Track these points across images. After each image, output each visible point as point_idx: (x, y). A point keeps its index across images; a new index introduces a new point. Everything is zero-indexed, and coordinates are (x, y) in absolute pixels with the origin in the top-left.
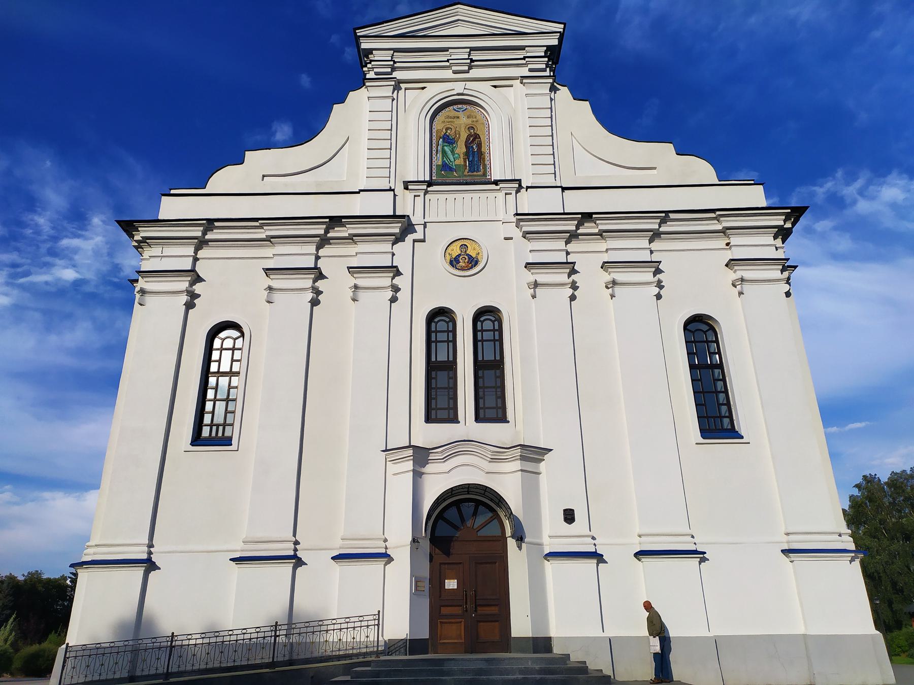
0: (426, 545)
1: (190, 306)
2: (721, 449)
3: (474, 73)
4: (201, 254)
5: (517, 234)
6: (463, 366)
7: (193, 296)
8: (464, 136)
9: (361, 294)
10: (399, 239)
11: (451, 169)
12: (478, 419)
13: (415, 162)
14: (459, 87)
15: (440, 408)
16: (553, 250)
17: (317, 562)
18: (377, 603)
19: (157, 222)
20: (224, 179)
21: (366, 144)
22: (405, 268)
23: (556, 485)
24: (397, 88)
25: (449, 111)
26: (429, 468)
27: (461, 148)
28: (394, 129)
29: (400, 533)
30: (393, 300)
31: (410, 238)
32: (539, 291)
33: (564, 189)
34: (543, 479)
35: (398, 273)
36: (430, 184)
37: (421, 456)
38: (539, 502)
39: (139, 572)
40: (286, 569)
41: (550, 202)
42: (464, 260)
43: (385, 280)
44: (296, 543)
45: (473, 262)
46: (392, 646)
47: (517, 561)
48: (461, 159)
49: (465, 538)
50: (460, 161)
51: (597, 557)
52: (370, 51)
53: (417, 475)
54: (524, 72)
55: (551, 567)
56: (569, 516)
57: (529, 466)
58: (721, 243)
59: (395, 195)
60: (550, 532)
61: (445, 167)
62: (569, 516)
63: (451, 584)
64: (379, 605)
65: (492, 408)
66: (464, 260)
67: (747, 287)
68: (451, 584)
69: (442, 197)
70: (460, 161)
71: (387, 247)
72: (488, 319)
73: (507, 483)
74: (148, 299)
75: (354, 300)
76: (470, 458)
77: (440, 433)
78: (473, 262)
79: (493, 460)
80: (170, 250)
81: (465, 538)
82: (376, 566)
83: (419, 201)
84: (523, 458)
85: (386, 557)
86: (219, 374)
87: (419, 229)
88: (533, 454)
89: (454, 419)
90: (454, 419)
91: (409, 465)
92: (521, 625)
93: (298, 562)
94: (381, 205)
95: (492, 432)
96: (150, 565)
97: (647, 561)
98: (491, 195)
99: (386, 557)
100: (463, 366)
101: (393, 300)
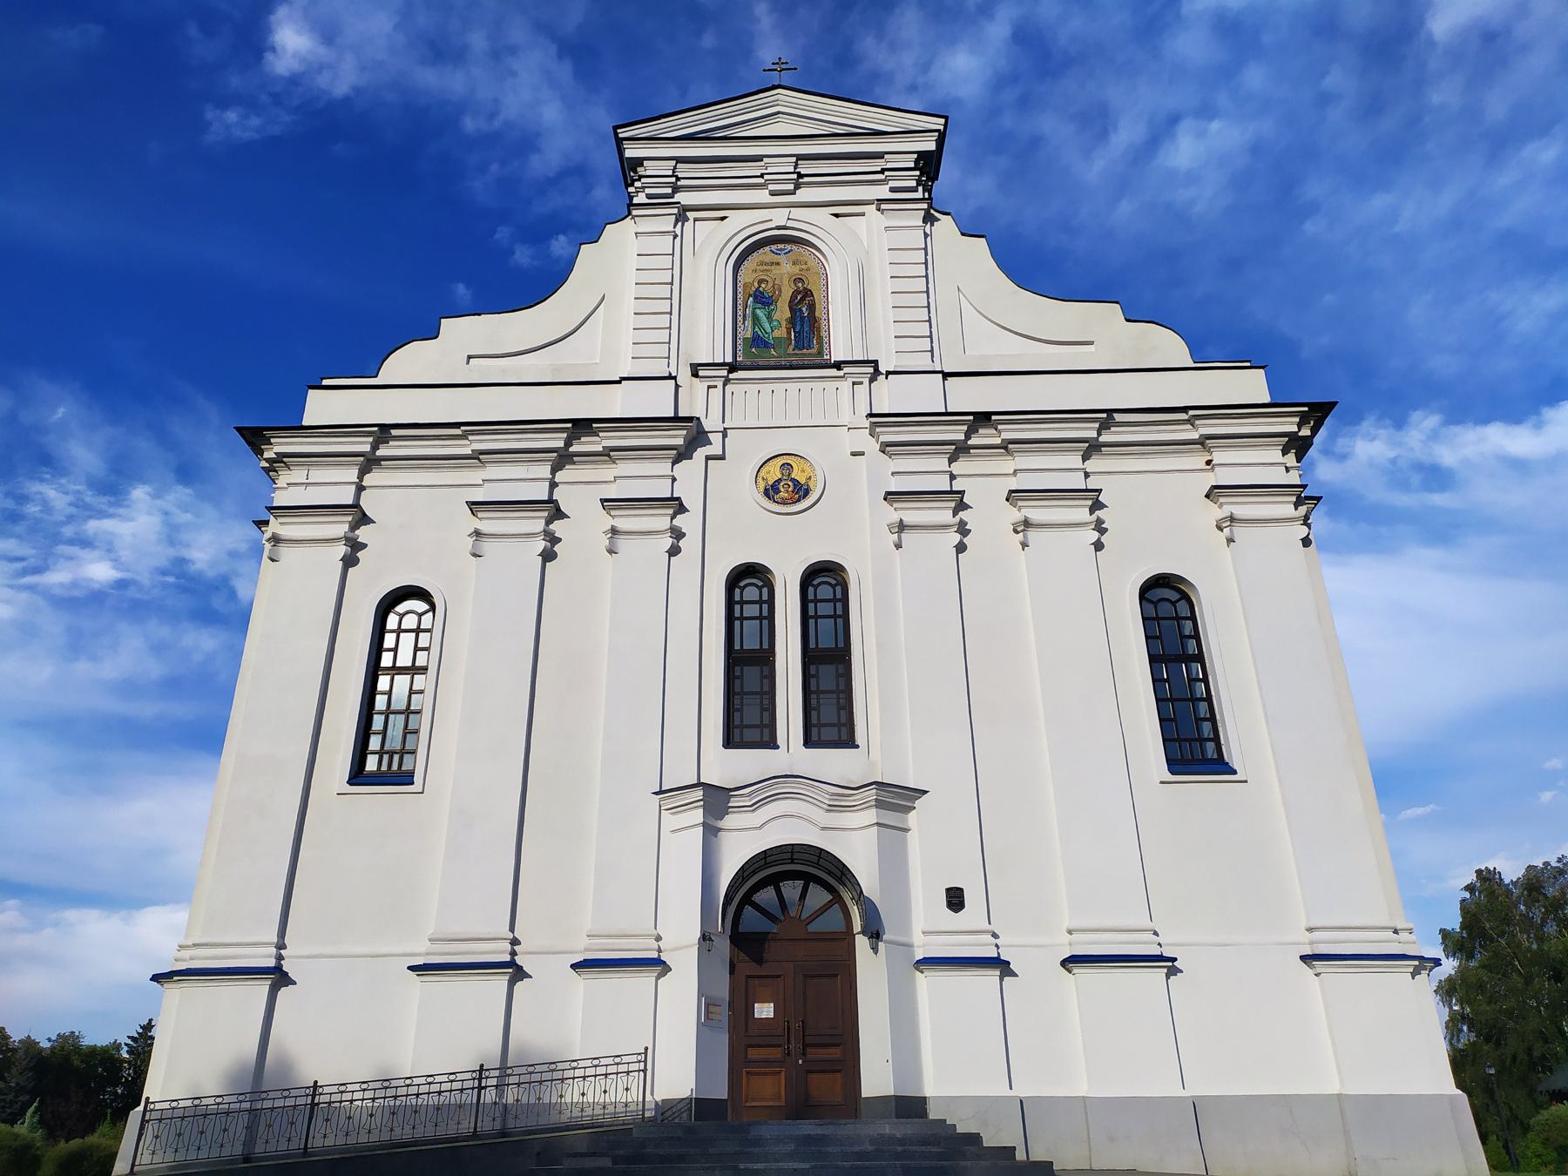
0: (723, 946)
1: (349, 561)
2: (1201, 791)
3: (804, 195)
4: (368, 480)
5: (872, 446)
6: (788, 658)
7: (355, 546)
8: (787, 292)
9: (623, 543)
10: (683, 454)
11: (766, 345)
12: (808, 742)
13: (710, 334)
14: (779, 217)
15: (747, 723)
16: (929, 471)
17: (547, 969)
18: (650, 1044)
19: (299, 429)
20: (406, 362)
21: (630, 305)
22: (692, 500)
23: (934, 849)
24: (681, 218)
25: (765, 254)
26: (729, 821)
27: (782, 312)
28: (676, 283)
29: (681, 928)
30: (674, 551)
31: (700, 453)
32: (907, 537)
33: (946, 375)
34: (913, 839)
35: (681, 509)
36: (733, 368)
37: (717, 800)
38: (909, 877)
39: (262, 988)
40: (500, 982)
41: (924, 395)
42: (788, 489)
43: (660, 520)
44: (515, 942)
45: (801, 491)
46: (667, 1109)
47: (872, 971)
48: (783, 328)
49: (786, 936)
50: (781, 333)
51: (1000, 965)
52: (639, 162)
53: (711, 832)
54: (883, 192)
55: (927, 984)
56: (955, 899)
57: (891, 818)
58: (1198, 461)
59: (677, 386)
60: (925, 925)
61: (757, 341)
62: (955, 899)
63: (764, 1011)
64: (650, 1044)
65: (831, 722)
66: (788, 489)
67: (1239, 531)
68: (764, 1011)
69: (752, 389)
70: (781, 333)
71: (664, 467)
72: (825, 582)
73: (855, 844)
74: (285, 551)
75: (611, 551)
76: (796, 801)
77: (747, 764)
78: (801, 491)
79: (832, 808)
80: (318, 474)
81: (786, 936)
82: (643, 981)
83: (716, 394)
84: (879, 804)
85: (658, 965)
86: (395, 670)
87: (716, 439)
88: (897, 798)
89: (772, 744)
90: (772, 744)
91: (697, 815)
92: (876, 1079)
93: (518, 973)
94: (657, 401)
95: (832, 763)
96: (279, 977)
97: (1083, 973)
98: (830, 386)
99: (658, 965)
100: (788, 658)
101: (674, 551)
